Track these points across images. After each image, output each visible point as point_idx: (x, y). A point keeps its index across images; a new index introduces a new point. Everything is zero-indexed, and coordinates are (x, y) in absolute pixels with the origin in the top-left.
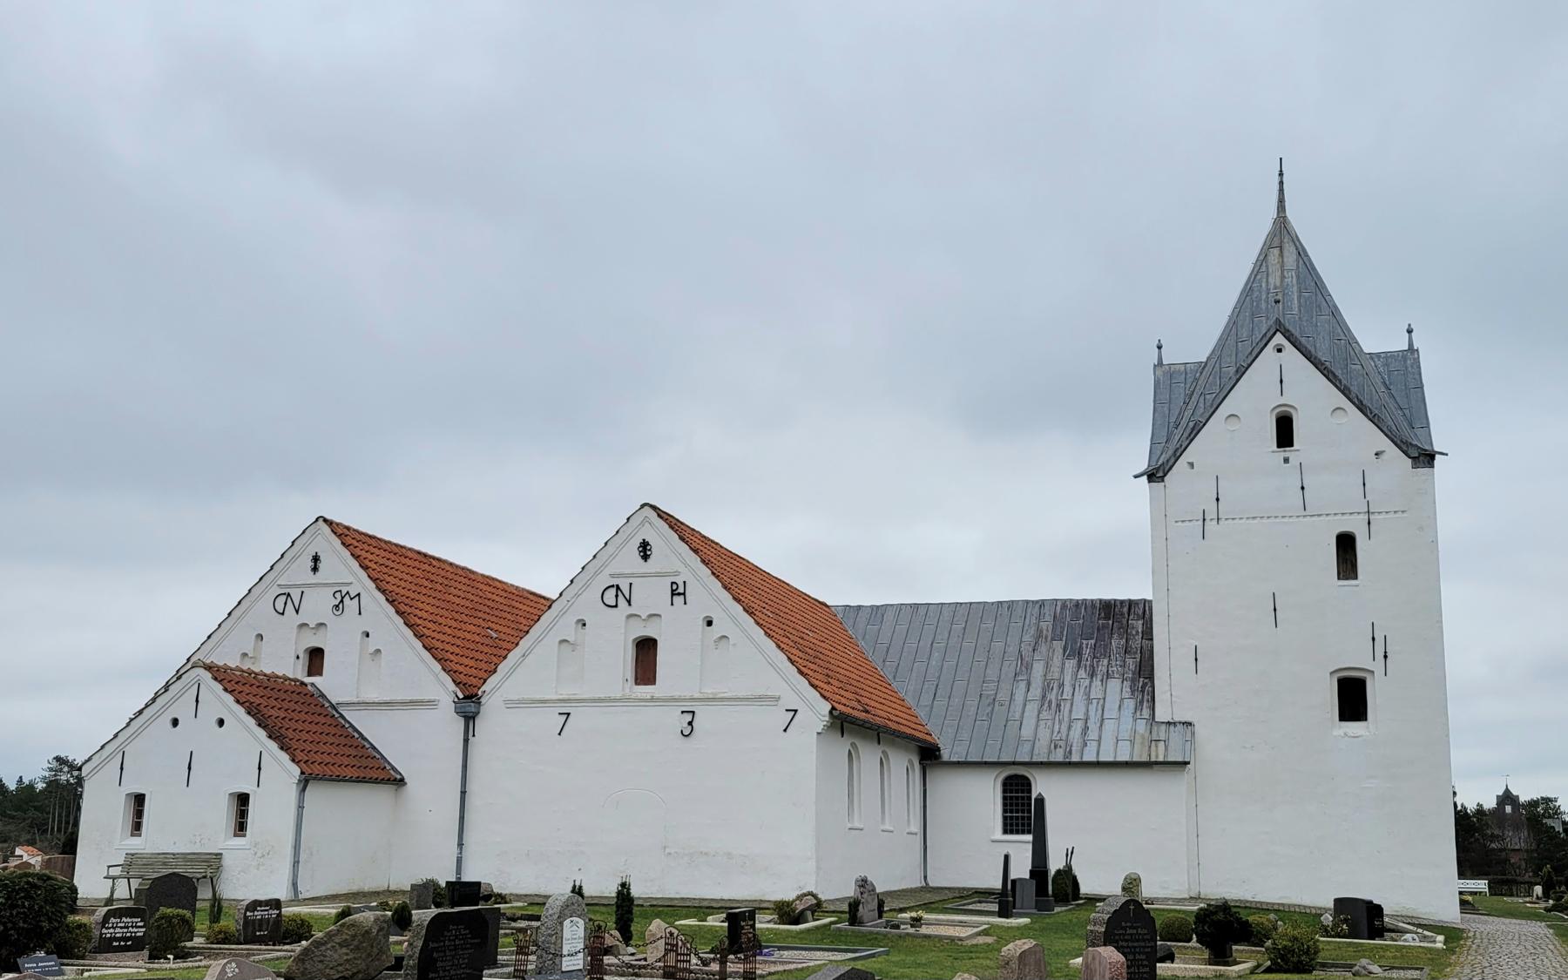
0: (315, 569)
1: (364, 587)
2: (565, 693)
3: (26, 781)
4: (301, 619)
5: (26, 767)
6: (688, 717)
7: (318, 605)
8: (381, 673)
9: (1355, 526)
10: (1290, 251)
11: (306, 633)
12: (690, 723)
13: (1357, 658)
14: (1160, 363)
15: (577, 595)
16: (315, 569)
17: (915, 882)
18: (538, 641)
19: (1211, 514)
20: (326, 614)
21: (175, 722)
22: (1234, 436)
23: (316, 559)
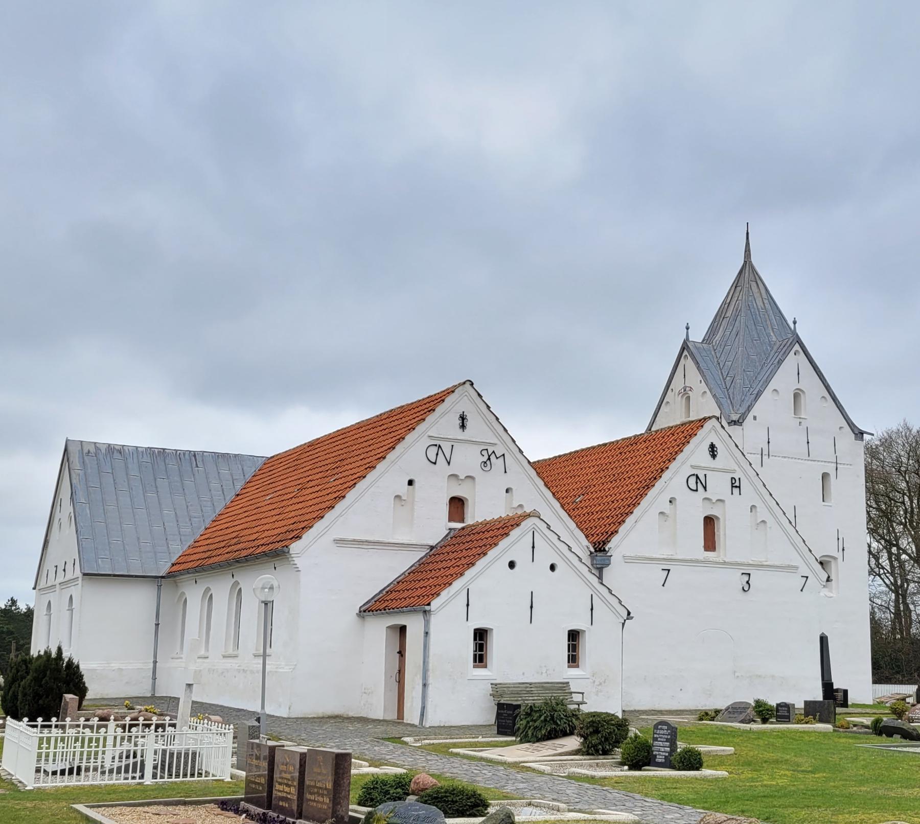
0: (463, 426)
2: (664, 552)
4: (452, 470)
6: (746, 578)
7: (718, 485)
9: (830, 469)
11: (454, 482)
12: (748, 582)
16: (463, 426)
17: (144, 690)
18: (645, 512)
20: (476, 471)
21: (512, 565)
23: (463, 418)
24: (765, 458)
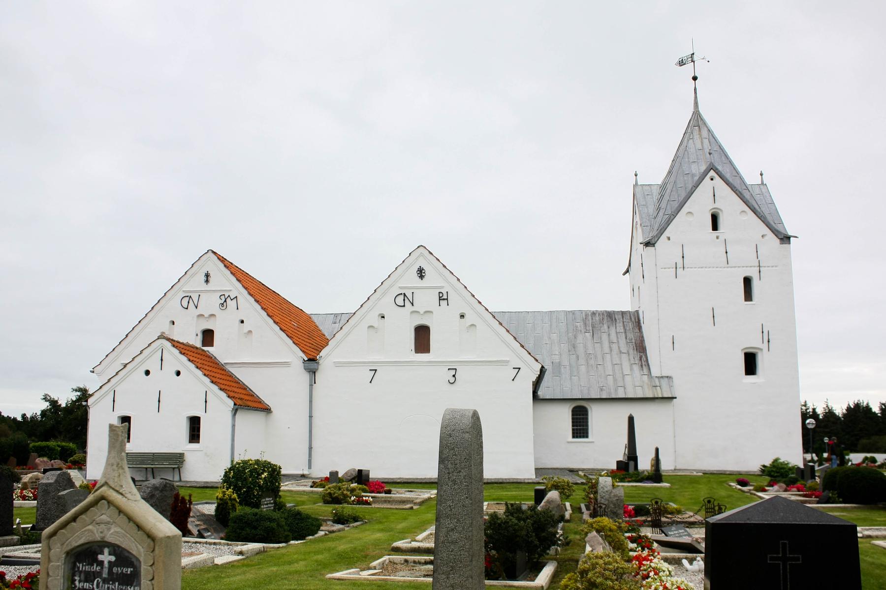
0: (207, 281)
1: (240, 293)
3: (29, 416)
5: (25, 404)
6: (453, 372)
7: (209, 303)
8: (254, 347)
9: (752, 273)
10: (705, 133)
11: (201, 320)
12: (454, 376)
13: (753, 342)
14: (636, 185)
15: (379, 299)
16: (207, 281)
19: (680, 265)
20: (216, 310)
21: (147, 373)
22: (691, 223)
23: (207, 275)
24: (680, 271)
